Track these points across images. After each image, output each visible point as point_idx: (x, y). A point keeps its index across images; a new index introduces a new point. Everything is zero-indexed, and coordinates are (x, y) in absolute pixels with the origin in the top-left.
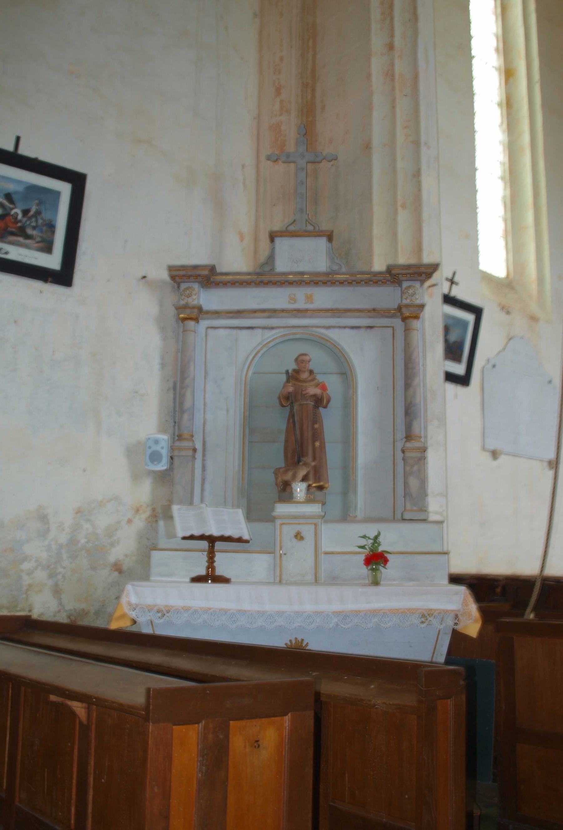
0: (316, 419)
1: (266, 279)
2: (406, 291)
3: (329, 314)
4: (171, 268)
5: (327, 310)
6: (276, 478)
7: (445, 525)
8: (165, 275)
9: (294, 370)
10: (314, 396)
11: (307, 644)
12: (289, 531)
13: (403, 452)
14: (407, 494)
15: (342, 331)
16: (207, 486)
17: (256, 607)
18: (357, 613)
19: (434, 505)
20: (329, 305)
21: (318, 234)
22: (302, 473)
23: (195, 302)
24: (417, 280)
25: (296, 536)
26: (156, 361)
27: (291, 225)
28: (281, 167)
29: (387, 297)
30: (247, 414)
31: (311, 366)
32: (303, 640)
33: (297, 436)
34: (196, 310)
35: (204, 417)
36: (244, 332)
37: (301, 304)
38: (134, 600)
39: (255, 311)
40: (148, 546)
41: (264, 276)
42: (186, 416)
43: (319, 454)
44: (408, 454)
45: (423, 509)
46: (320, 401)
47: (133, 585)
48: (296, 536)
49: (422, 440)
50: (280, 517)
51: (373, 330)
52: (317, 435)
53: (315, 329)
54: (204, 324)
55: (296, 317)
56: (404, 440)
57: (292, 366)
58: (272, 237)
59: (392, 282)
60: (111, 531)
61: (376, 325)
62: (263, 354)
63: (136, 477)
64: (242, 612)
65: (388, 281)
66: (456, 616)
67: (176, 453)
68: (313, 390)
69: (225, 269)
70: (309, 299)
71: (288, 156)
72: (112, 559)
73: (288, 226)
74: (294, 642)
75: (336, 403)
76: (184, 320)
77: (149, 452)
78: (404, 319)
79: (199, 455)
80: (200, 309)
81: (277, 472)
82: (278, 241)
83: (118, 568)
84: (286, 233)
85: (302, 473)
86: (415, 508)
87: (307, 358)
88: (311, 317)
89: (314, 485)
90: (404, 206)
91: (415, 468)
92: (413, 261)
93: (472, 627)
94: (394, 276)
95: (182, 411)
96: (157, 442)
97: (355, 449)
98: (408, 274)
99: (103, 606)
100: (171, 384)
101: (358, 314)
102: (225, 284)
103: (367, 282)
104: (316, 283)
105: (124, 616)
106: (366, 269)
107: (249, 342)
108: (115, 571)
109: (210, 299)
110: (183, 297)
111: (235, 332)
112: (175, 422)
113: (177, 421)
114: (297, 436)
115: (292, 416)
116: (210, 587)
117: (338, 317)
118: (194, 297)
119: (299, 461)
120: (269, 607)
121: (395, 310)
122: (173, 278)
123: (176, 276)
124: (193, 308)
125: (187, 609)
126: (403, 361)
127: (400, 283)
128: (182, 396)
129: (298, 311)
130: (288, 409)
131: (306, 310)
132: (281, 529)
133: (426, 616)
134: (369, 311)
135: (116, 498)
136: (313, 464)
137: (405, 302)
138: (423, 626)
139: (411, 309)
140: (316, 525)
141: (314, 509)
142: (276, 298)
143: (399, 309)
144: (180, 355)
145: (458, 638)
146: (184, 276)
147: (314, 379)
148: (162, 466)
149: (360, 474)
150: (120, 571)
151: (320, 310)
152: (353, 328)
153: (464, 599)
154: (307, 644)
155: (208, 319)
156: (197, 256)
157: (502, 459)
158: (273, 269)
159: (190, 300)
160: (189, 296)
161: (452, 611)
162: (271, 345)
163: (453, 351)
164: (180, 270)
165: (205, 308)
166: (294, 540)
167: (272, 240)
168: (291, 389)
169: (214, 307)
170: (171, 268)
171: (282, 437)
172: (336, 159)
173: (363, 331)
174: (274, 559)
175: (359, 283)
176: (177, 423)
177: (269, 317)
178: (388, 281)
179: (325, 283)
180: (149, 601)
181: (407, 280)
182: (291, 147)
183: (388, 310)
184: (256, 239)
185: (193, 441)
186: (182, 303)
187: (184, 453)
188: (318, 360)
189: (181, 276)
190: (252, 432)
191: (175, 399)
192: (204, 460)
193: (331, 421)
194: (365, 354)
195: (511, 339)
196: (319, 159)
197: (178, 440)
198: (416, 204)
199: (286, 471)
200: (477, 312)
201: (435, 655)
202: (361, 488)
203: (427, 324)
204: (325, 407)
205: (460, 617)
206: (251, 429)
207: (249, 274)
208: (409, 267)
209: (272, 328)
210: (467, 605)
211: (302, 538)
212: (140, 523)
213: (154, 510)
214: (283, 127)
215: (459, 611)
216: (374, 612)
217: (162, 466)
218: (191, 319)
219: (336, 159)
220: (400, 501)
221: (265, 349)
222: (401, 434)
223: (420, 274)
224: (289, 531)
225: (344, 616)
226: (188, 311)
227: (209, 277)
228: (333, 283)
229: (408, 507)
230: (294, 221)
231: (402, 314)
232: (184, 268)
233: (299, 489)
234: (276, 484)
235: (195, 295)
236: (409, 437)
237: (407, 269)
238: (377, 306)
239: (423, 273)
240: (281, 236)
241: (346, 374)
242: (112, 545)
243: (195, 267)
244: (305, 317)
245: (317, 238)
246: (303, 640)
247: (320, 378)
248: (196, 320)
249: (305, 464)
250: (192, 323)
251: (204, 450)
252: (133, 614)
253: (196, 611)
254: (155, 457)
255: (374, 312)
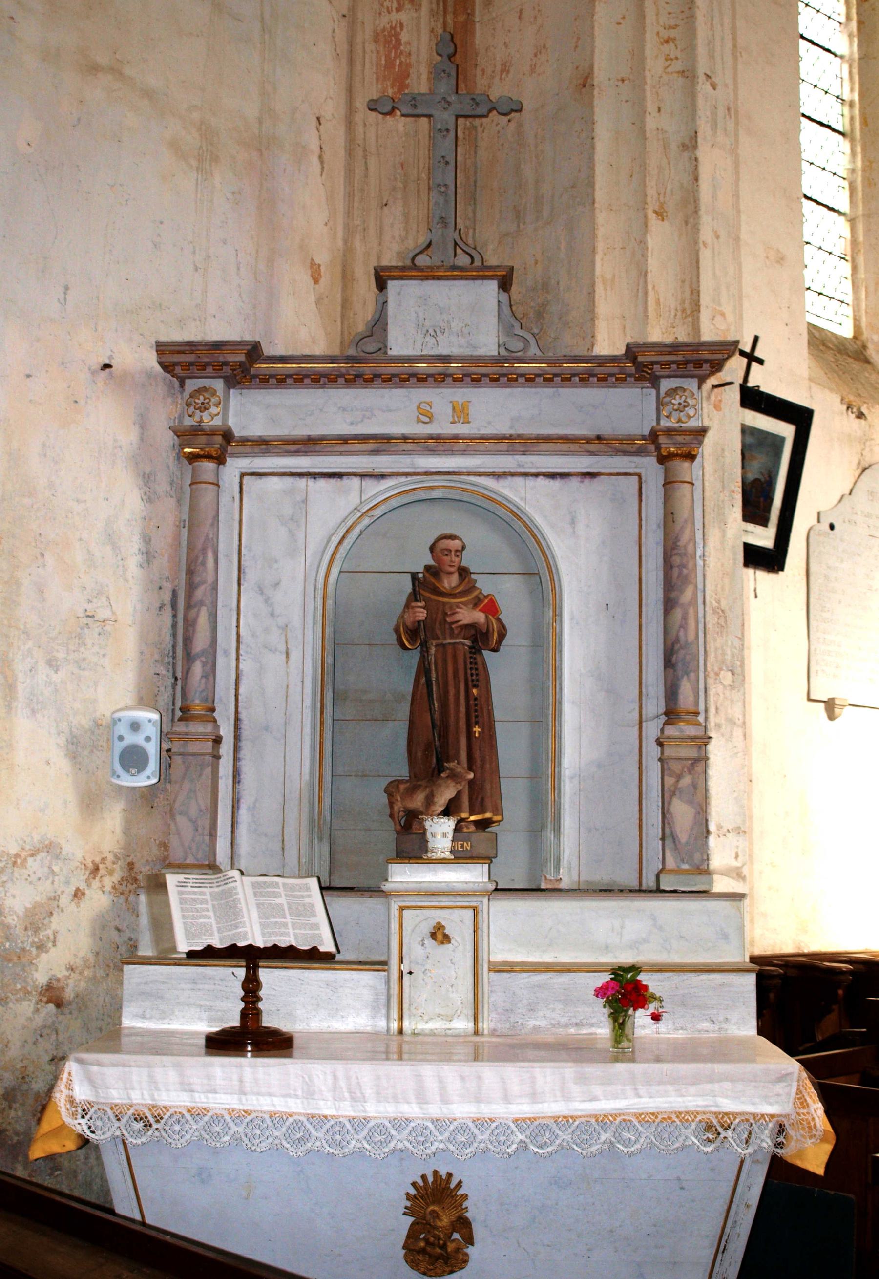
0: (477, 678)
1: (367, 369)
2: (667, 399)
3: (503, 446)
4: (161, 348)
5: (500, 438)
6: (391, 804)
7: (747, 901)
8: (151, 360)
9: (428, 568)
10: (473, 626)
11: (459, 1184)
12: (417, 923)
13: (660, 744)
14: (667, 836)
15: (531, 482)
16: (244, 814)
17: (347, 1110)
18: (566, 1120)
19: (720, 853)
20: (503, 428)
21: (477, 271)
22: (446, 794)
23: (217, 422)
24: (692, 377)
25: (433, 935)
26: (133, 546)
27: (421, 252)
28: (399, 124)
29: (628, 409)
30: (329, 660)
31: (467, 560)
32: (450, 1175)
33: (437, 721)
34: (219, 439)
35: (237, 667)
36: (322, 483)
37: (443, 427)
38: (82, 1092)
39: (344, 440)
40: (120, 953)
41: (362, 364)
42: (197, 669)
43: (483, 755)
44: (669, 752)
45: (703, 870)
46: (485, 638)
47: (80, 1061)
48: (433, 935)
49: (701, 718)
50: (399, 894)
51: (596, 480)
52: (480, 711)
53: (472, 479)
54: (235, 466)
55: (432, 452)
56: (663, 718)
57: (421, 560)
58: (381, 280)
59: (637, 379)
60: (37, 918)
61: (602, 471)
62: (360, 363)
63: (90, 802)
64: (317, 1120)
65: (630, 375)
66: (781, 1129)
67: (176, 747)
68: (468, 615)
69: (279, 350)
70: (461, 413)
71: (414, 101)
72: (41, 978)
73: (416, 255)
74: (430, 1179)
75: (517, 639)
76: (192, 458)
77: (119, 747)
78: (662, 460)
79: (226, 749)
80: (228, 436)
81: (391, 790)
82: (393, 286)
83: (52, 994)
84: (411, 270)
85: (446, 794)
86: (685, 866)
87: (455, 544)
88: (464, 453)
89: (472, 818)
90: (660, 214)
91: (686, 780)
92: (682, 335)
93: (814, 1155)
94: (640, 366)
95: (189, 658)
96: (135, 726)
97: (557, 736)
98: (674, 362)
99: (23, 1078)
100: (167, 597)
101: (565, 447)
102: (282, 381)
103: (585, 379)
104: (476, 380)
105: (63, 1127)
106: (582, 351)
107: (331, 507)
108: (47, 1002)
109: (248, 412)
110: (191, 410)
111: (302, 482)
112: (176, 679)
113: (179, 675)
114: (437, 721)
115: (423, 669)
116: (250, 1068)
117: (524, 453)
118: (214, 410)
119: (440, 769)
120: (376, 1109)
121: (643, 438)
122: (167, 367)
123: (175, 364)
124: (213, 433)
125: (197, 1113)
126: (661, 549)
127: (654, 381)
128: (190, 624)
129: (438, 438)
130: (413, 658)
131: (456, 438)
132: (401, 917)
133: (715, 1127)
134: (588, 441)
135: (50, 848)
136: (471, 776)
137: (665, 423)
138: (709, 1149)
139: (680, 439)
140: (475, 909)
141: (471, 875)
142: (389, 410)
143: (653, 436)
144: (185, 532)
145: (781, 1173)
146: (191, 364)
147: (472, 588)
148: (147, 778)
149: (568, 788)
150: (59, 1004)
151: (484, 438)
152: (552, 476)
153: (799, 1091)
154: (459, 1184)
155: (246, 455)
156: (223, 322)
157: (846, 715)
158: (383, 348)
159: (206, 417)
160: (204, 408)
161: (772, 1116)
162: (378, 512)
163: (755, 508)
164: (183, 352)
165: (238, 433)
166: (429, 942)
167: (381, 285)
168: (422, 615)
169: (256, 430)
170: (161, 348)
171: (404, 710)
172: (520, 111)
173: (574, 482)
174: (388, 982)
175: (567, 379)
176: (180, 680)
177: (376, 452)
178: (630, 375)
179: (495, 380)
180: (116, 1096)
181: (669, 377)
182: (420, 82)
183: (631, 439)
184: (346, 277)
185: (215, 721)
186: (188, 422)
187: (193, 747)
188: (482, 548)
189: (184, 362)
190: (339, 697)
191: (174, 626)
192: (236, 759)
193: (506, 674)
194: (582, 538)
195: (865, 469)
196: (480, 111)
197: (180, 719)
198: (689, 208)
199: (412, 790)
200: (801, 418)
201: (734, 1207)
202: (568, 823)
203: (709, 469)
204: (495, 650)
205: (791, 1132)
206: (335, 692)
207: (332, 359)
208: (675, 348)
209: (383, 476)
210: (804, 1104)
211: (446, 939)
212: (99, 899)
213: (131, 866)
214: (404, 37)
215: (787, 1116)
216: (603, 1120)
217: (149, 777)
218: (209, 457)
219: (520, 111)
220: (653, 846)
221: (366, 521)
222: (655, 705)
223: (698, 364)
224: (417, 923)
225: (535, 1127)
226: (203, 439)
227: (245, 365)
228: (512, 380)
229: (671, 863)
230: (429, 245)
231: (658, 448)
232: (191, 346)
233: (441, 832)
234: (391, 816)
235: (217, 405)
236: (671, 715)
237: (670, 353)
238: (606, 430)
239: (706, 361)
240: (401, 278)
241: (540, 575)
242: (41, 947)
243: (218, 346)
244: (452, 453)
245: (478, 282)
246: (450, 1175)
247: (485, 585)
248: (220, 460)
249: (454, 776)
250: (209, 466)
251: (237, 738)
252: (81, 1126)
253: (217, 1118)
254: (133, 759)
255: (598, 443)
